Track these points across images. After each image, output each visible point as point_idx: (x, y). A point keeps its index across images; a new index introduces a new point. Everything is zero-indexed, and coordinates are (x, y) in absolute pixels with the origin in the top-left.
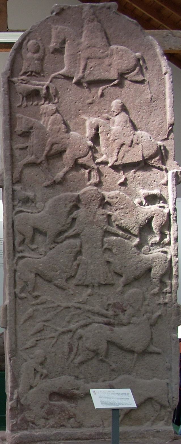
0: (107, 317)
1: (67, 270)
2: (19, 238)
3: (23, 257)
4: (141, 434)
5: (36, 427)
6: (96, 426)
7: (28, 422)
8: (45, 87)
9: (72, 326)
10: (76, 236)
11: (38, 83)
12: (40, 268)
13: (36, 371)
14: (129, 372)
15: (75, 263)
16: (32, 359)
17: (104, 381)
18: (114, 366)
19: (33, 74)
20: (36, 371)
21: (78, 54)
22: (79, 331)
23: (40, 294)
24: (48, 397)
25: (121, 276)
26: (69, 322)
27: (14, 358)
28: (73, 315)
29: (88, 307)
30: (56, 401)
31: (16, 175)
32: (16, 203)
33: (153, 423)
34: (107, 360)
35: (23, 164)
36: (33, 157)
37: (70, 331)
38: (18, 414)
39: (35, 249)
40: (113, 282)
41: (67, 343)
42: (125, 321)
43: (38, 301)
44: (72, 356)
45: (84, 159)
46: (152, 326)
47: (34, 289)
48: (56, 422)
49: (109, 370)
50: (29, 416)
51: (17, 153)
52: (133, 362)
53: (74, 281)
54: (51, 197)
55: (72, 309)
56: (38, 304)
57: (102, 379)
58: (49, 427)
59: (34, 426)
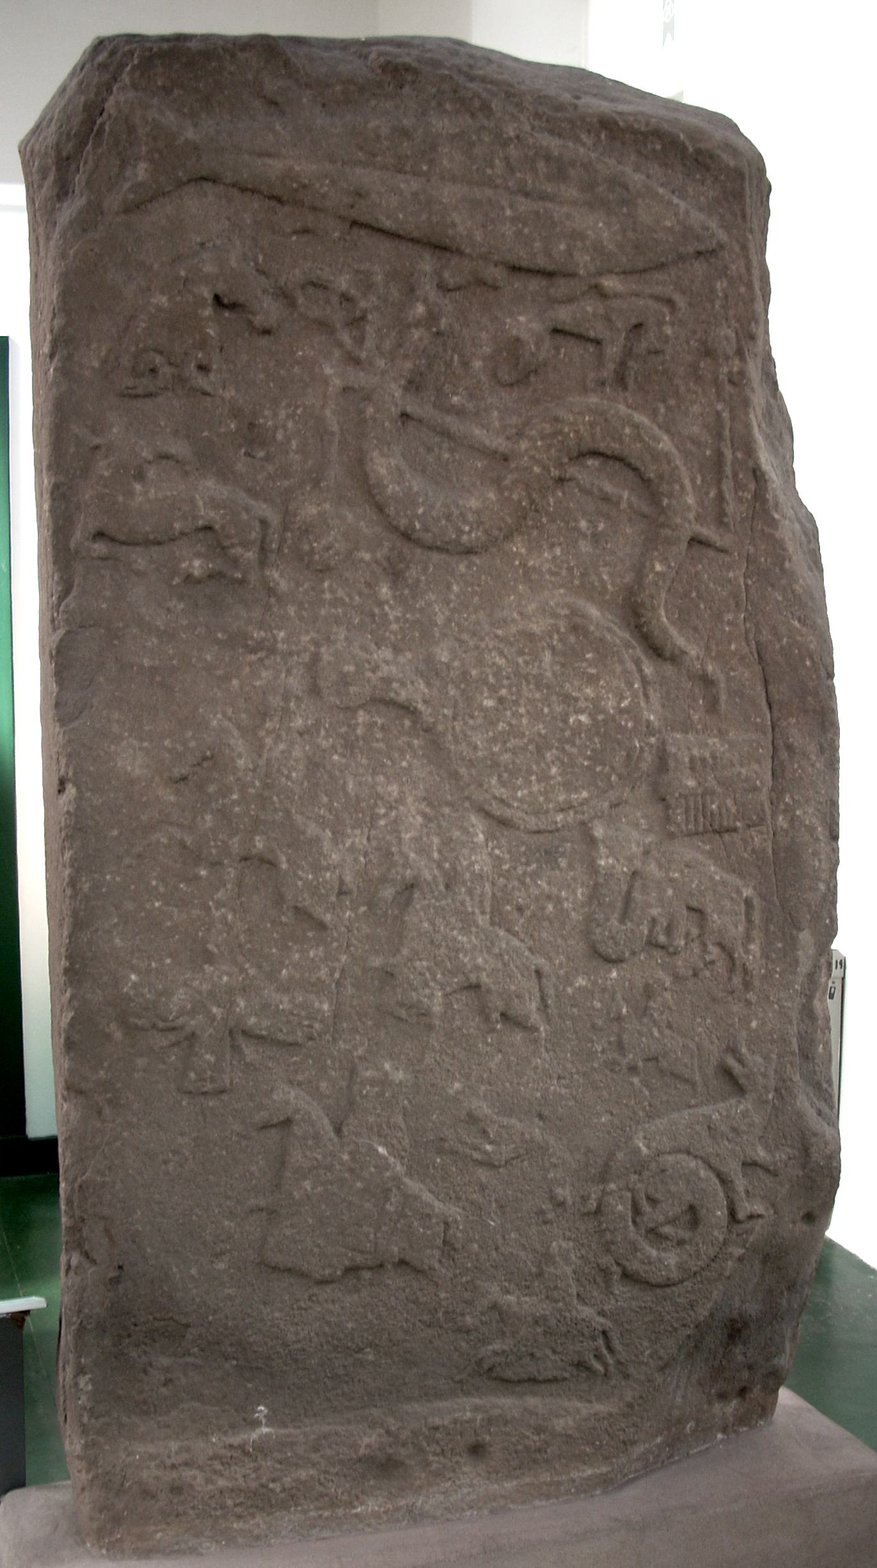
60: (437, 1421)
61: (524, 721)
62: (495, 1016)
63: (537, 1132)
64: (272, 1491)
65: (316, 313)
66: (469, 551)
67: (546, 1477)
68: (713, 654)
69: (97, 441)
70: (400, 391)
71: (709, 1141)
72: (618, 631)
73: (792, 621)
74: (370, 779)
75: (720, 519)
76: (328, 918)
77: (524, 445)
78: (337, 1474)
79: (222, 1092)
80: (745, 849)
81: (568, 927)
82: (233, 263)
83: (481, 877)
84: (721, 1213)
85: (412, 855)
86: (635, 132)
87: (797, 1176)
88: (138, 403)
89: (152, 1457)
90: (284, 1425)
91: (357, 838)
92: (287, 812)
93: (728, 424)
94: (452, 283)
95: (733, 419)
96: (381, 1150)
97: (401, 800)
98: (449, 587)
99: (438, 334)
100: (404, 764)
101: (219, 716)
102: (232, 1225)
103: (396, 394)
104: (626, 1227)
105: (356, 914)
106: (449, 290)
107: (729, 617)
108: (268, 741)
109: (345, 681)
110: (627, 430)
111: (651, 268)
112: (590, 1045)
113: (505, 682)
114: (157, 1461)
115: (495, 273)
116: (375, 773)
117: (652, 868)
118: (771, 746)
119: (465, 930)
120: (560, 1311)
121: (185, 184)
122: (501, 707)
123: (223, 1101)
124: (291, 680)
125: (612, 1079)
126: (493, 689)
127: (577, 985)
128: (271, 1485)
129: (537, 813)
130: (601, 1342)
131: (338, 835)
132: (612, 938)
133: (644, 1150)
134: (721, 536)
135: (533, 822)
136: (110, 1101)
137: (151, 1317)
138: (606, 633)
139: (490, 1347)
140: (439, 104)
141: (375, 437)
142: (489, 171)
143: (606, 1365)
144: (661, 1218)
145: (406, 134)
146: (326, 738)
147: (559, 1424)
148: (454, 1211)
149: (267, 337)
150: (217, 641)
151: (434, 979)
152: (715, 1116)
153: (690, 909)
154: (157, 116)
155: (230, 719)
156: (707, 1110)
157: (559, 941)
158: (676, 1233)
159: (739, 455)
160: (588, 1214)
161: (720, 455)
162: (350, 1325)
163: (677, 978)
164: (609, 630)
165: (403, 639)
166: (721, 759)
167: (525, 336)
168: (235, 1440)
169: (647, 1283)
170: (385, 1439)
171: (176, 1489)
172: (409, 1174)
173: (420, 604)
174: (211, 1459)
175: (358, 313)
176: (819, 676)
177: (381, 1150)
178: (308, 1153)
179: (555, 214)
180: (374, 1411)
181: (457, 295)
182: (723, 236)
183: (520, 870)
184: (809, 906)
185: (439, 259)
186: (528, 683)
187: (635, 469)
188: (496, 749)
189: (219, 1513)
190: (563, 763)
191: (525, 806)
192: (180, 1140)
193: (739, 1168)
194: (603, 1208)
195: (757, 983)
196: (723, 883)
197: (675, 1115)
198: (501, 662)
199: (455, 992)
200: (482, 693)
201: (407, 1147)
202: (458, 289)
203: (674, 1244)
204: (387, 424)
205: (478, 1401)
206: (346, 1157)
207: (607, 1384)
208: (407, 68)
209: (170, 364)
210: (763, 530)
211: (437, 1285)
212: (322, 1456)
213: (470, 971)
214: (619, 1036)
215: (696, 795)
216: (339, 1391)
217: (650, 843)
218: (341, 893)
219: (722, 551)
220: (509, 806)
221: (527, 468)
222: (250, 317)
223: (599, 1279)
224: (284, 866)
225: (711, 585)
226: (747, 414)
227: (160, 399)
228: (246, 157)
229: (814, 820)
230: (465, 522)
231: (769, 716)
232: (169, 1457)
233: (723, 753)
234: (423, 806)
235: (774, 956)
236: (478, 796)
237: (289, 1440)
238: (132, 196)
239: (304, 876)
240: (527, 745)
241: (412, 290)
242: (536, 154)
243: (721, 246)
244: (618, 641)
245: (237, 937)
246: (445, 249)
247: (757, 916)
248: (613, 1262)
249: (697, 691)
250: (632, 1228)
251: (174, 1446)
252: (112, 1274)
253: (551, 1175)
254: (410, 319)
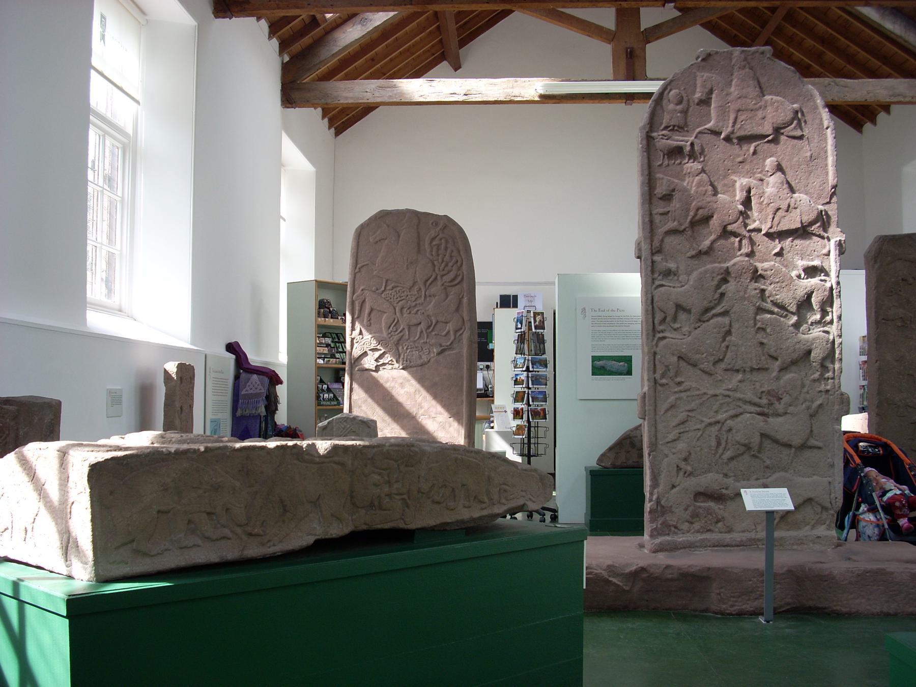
0: (760, 406)
1: (714, 352)
2: (659, 316)
3: (664, 338)
4: (799, 540)
5: (679, 532)
6: (748, 531)
7: (670, 526)
8: (689, 143)
9: (721, 417)
10: (725, 313)
11: (681, 138)
12: (683, 350)
13: (679, 469)
14: (785, 470)
15: (723, 345)
16: (674, 454)
17: (757, 479)
18: (768, 462)
19: (676, 128)
20: (679, 469)
21: (727, 105)
22: (728, 422)
23: (683, 380)
24: (692, 498)
25: (776, 359)
26: (716, 412)
27: (654, 453)
28: (721, 404)
29: (738, 395)
30: (702, 502)
31: (656, 243)
32: (656, 276)
33: (813, 527)
34: (760, 456)
35: (665, 231)
36: (676, 223)
37: (718, 422)
38: (658, 517)
39: (678, 328)
40: (767, 366)
41: (714, 436)
42: (781, 411)
43: (681, 388)
44: (720, 451)
45: (734, 225)
46: (811, 416)
47: (677, 374)
48: (702, 527)
49: (762, 467)
50: (671, 519)
51: (657, 219)
52: (791, 458)
53: (723, 366)
54: (696, 269)
55: (720, 397)
56: (681, 392)
57: (755, 477)
58: (694, 532)
59: (676, 530)
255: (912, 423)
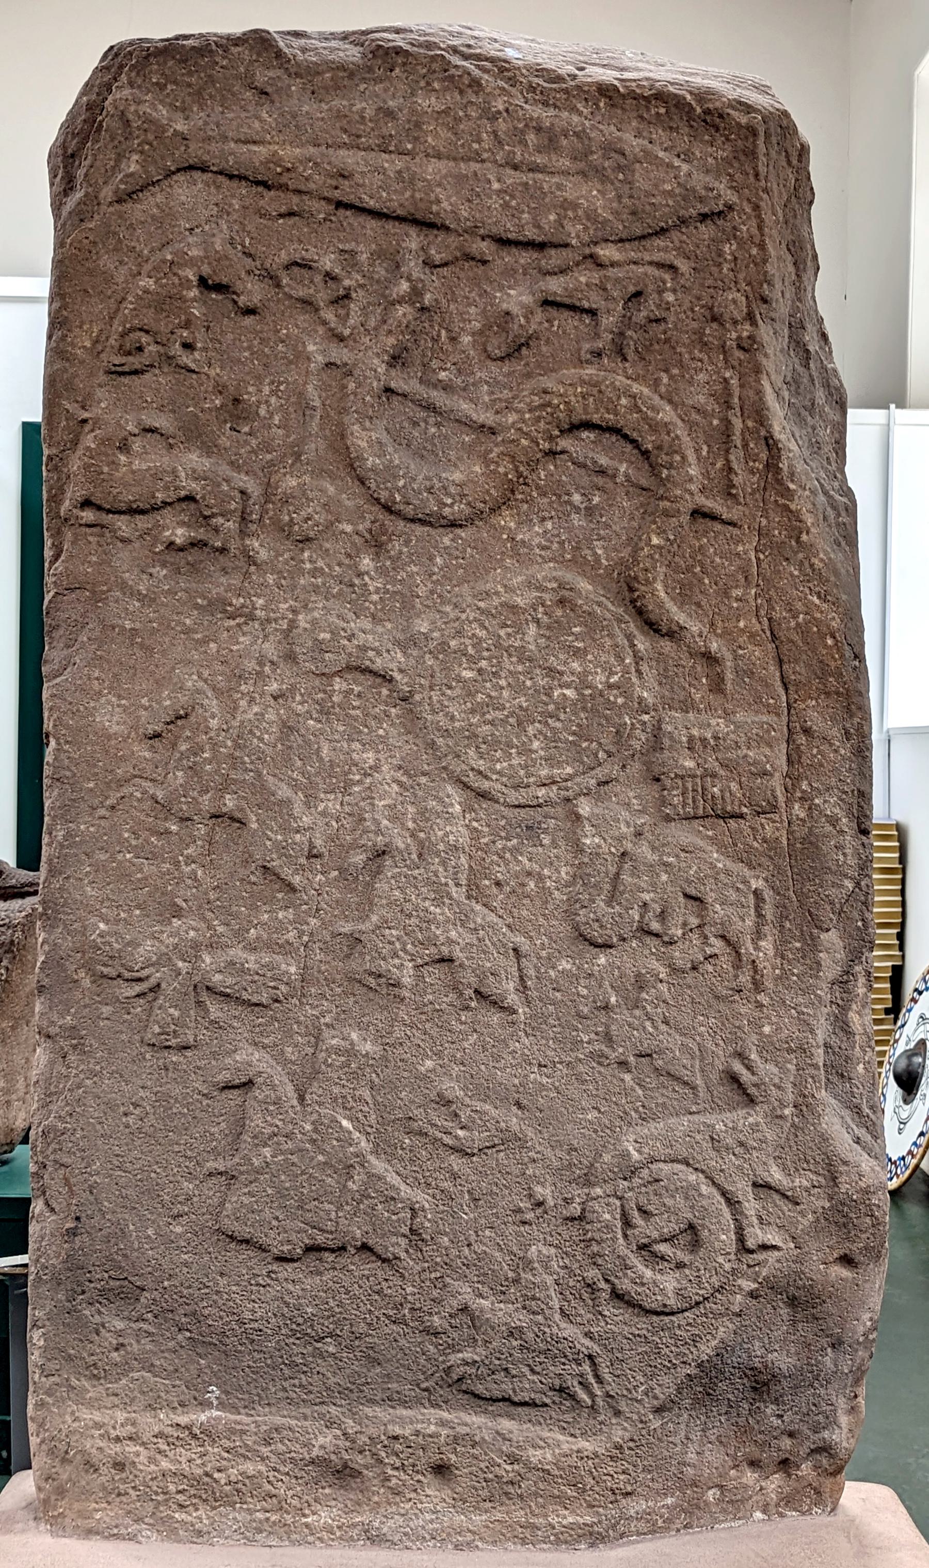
60: (398, 1431)
61: (505, 694)
62: (469, 992)
63: (514, 1121)
64: (216, 1481)
65: (301, 293)
66: (453, 524)
67: (520, 1515)
68: (719, 631)
69: (86, 415)
70: (383, 365)
71: (713, 1154)
72: (610, 605)
73: (810, 597)
74: (346, 746)
75: (729, 492)
76: (297, 880)
77: (512, 418)
78: (287, 1474)
79: (186, 1048)
80: (755, 839)
81: (550, 906)
82: (218, 247)
83: (457, 849)
84: (728, 1238)
85: (385, 822)
86: (636, 97)
87: (823, 1208)
88: (126, 380)
89: (98, 1426)
90: (235, 1410)
91: (332, 804)
92: (259, 774)
93: (736, 392)
94: (438, 258)
95: (742, 386)
96: (345, 1123)
97: (376, 768)
98: (431, 559)
99: (423, 309)
100: (381, 732)
101: (195, 677)
102: (191, 1186)
103: (379, 370)
104: (614, 1240)
105: (327, 879)
106: (436, 266)
107: (738, 592)
108: (243, 703)
109: (320, 648)
110: (624, 401)
111: (650, 235)
112: (574, 1033)
113: (486, 654)
114: (102, 1431)
115: (484, 247)
116: (350, 740)
117: (644, 851)
118: (785, 729)
119: (438, 902)
120: (538, 1324)
121: (174, 173)
122: (480, 678)
123: (186, 1057)
124: (267, 645)
125: (599, 1072)
126: (472, 660)
127: (560, 968)
128: (216, 1475)
129: (516, 787)
130: (586, 1367)
131: (310, 801)
132: (597, 921)
133: (635, 1156)
134: (728, 507)
135: (514, 797)
136: (74, 1047)
137: (106, 1275)
138: (596, 608)
139: (460, 1355)
140: (428, 84)
141: (355, 411)
142: (476, 146)
143: (592, 1396)
144: (655, 1235)
145: (390, 114)
146: (301, 703)
147: (535, 1456)
148: (421, 1198)
149: (252, 317)
150: (197, 606)
151: (404, 950)
152: (720, 1127)
153: (687, 896)
154: (148, 110)
155: (205, 681)
156: (710, 1119)
157: (541, 920)
158: (674, 1253)
159: (750, 424)
160: (573, 1219)
161: (727, 423)
162: (309, 1310)
163: (674, 970)
164: (599, 604)
165: (382, 609)
166: (724, 740)
167: (515, 310)
168: (183, 1420)
169: (640, 1306)
170: (342, 1443)
171: (119, 1466)
172: (375, 1152)
173: (402, 575)
174: (156, 1436)
175: (342, 292)
176: (842, 656)
177: (345, 1123)
178: (269, 1118)
179: (545, 186)
180: (332, 1409)
181: (445, 271)
182: (731, 197)
183: (499, 845)
184: (832, 903)
185: (426, 235)
186: (510, 655)
187: (633, 441)
188: (474, 721)
189: (160, 1498)
190: (546, 737)
191: (504, 779)
192: (142, 1093)
193: (749, 1189)
194: (587, 1214)
195: (769, 984)
196: (728, 873)
197: (672, 1120)
198: (482, 633)
199: (427, 964)
200: (460, 665)
201: (373, 1122)
202: (445, 264)
203: (672, 1266)
204: (368, 398)
205: (445, 1415)
206: (308, 1127)
207: (595, 1418)
208: (398, 51)
209: (157, 343)
210: (776, 501)
211: (402, 1276)
212: (271, 1451)
213: (442, 944)
214: (607, 1026)
215: (695, 776)
216: (296, 1382)
217: (643, 824)
218: (311, 856)
219: (729, 524)
220: (486, 777)
221: (513, 441)
222: (235, 297)
223: (586, 1296)
224: (254, 826)
225: (718, 560)
226: (758, 381)
227: (147, 376)
228: (232, 145)
229: (837, 810)
230: (448, 494)
231: (784, 698)
232: (114, 1428)
233: (728, 734)
234: (399, 775)
235: (790, 956)
236: (458, 767)
237: (238, 1427)
238: (123, 187)
239: (273, 836)
240: (507, 717)
241: (398, 267)
242: (526, 125)
243: (730, 208)
244: (608, 616)
245: (206, 894)
246: (432, 225)
247: (769, 911)
248: (600, 1277)
249: (699, 669)
250: (621, 1241)
251: (121, 1416)
252: (70, 1225)
253: (529, 1172)
254: (395, 296)
255: (228, 1087)
